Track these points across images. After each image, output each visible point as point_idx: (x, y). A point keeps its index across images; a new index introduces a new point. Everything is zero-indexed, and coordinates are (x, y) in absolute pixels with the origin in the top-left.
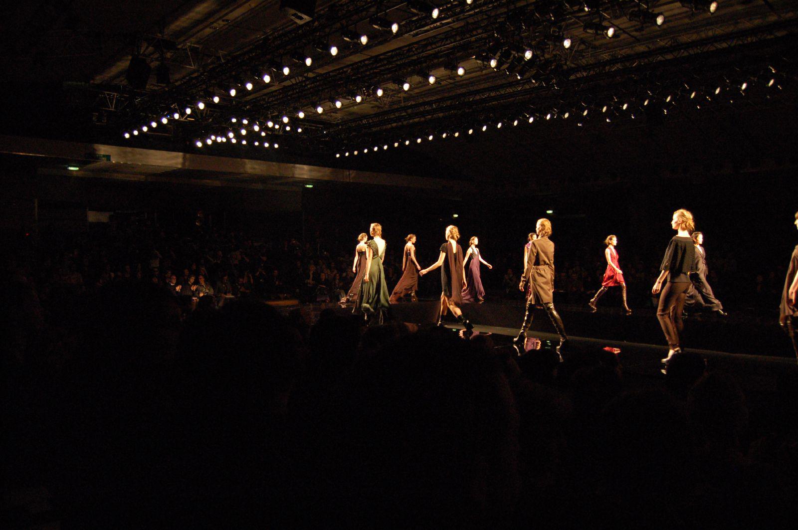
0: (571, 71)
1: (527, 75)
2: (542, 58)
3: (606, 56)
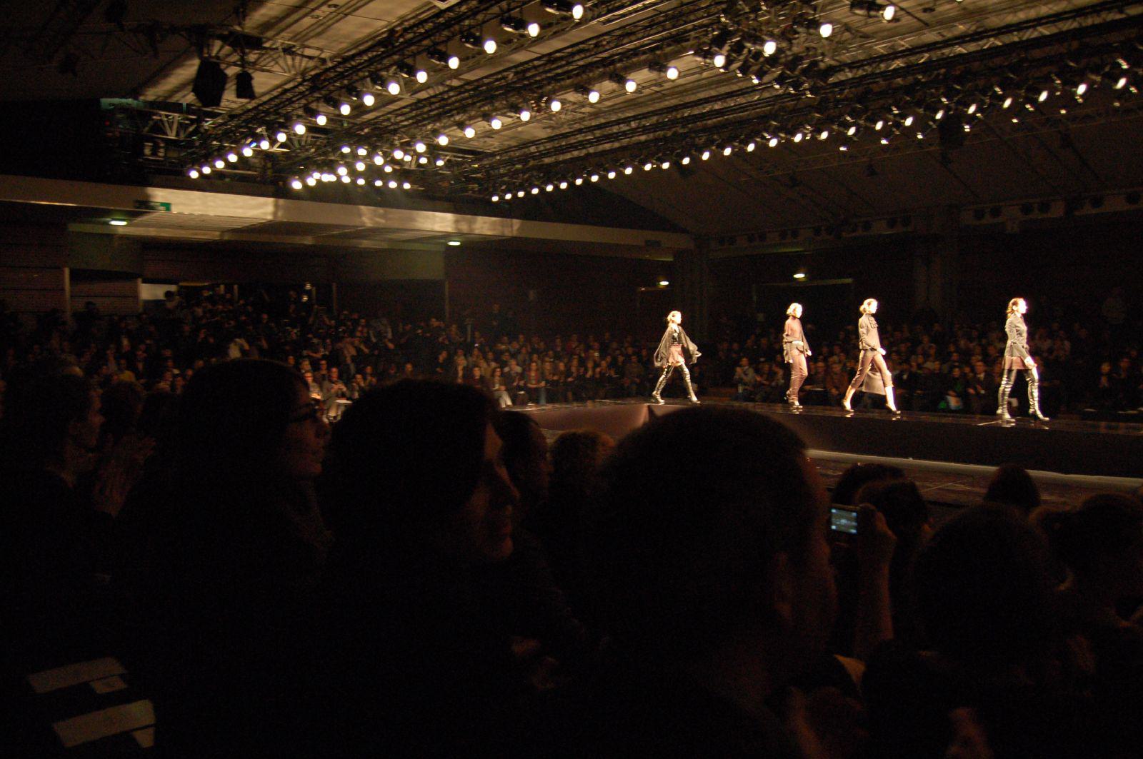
0: (831, 70)
1: (766, 79)
2: (788, 53)
3: (880, 48)
